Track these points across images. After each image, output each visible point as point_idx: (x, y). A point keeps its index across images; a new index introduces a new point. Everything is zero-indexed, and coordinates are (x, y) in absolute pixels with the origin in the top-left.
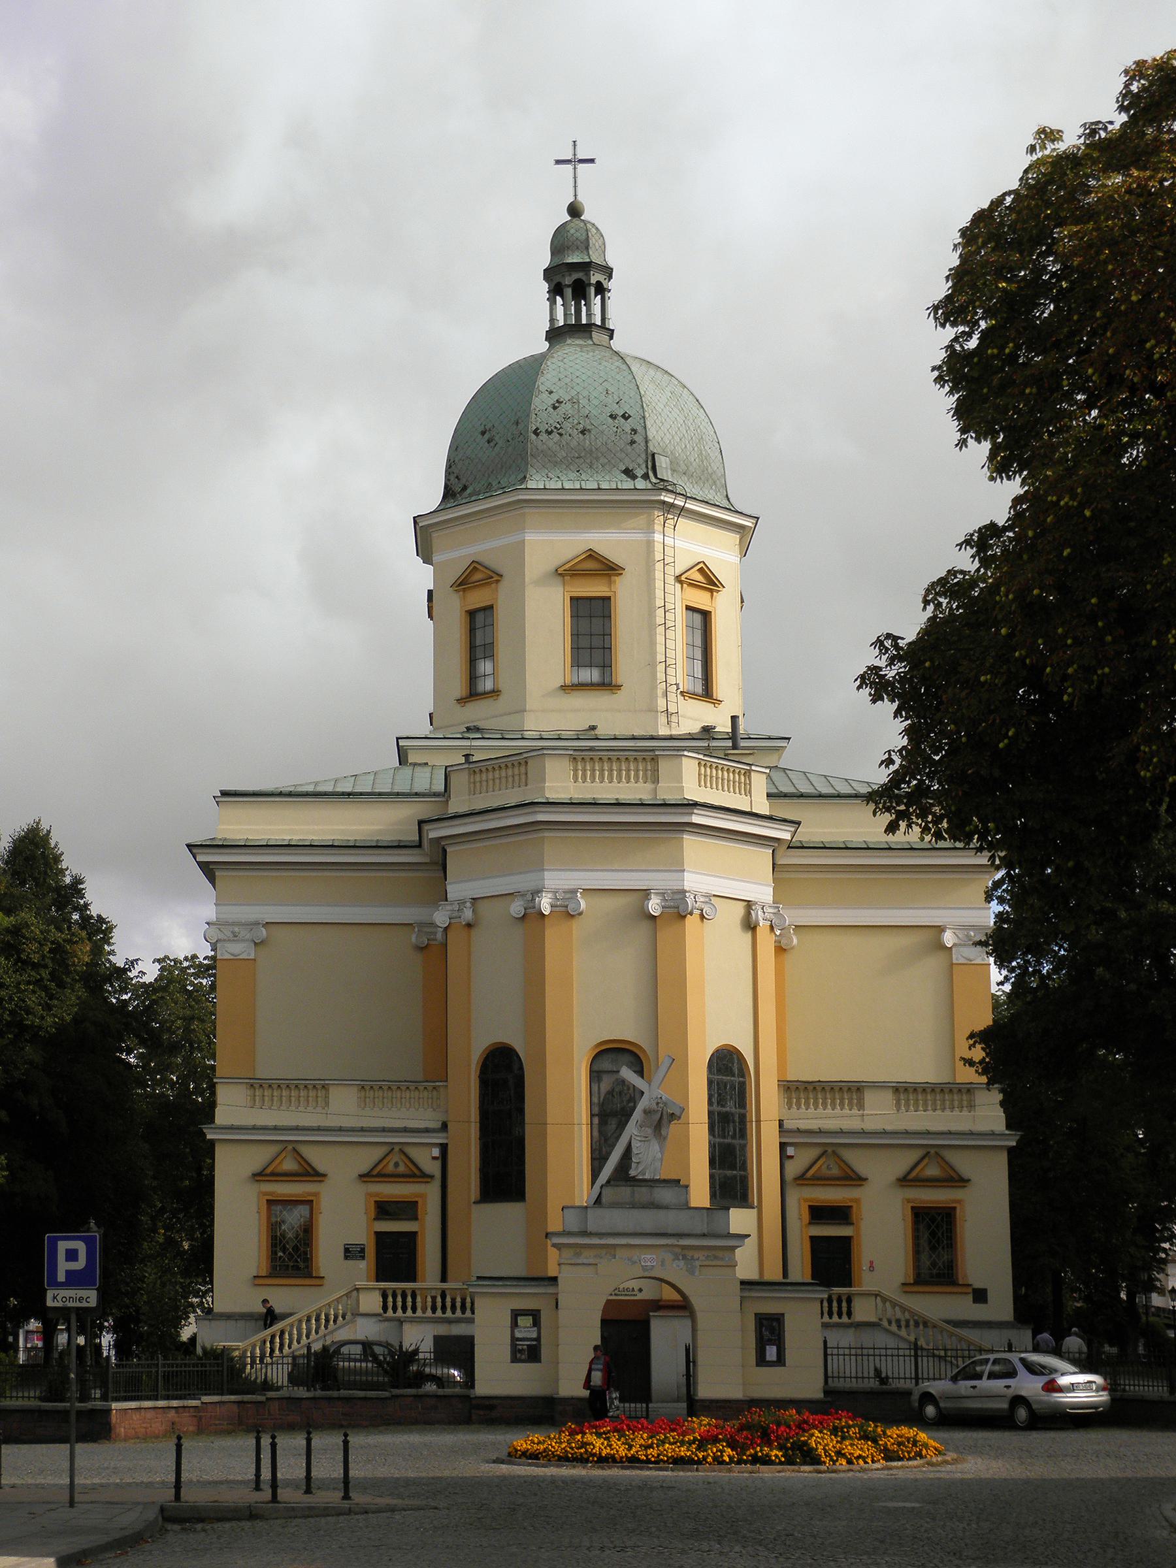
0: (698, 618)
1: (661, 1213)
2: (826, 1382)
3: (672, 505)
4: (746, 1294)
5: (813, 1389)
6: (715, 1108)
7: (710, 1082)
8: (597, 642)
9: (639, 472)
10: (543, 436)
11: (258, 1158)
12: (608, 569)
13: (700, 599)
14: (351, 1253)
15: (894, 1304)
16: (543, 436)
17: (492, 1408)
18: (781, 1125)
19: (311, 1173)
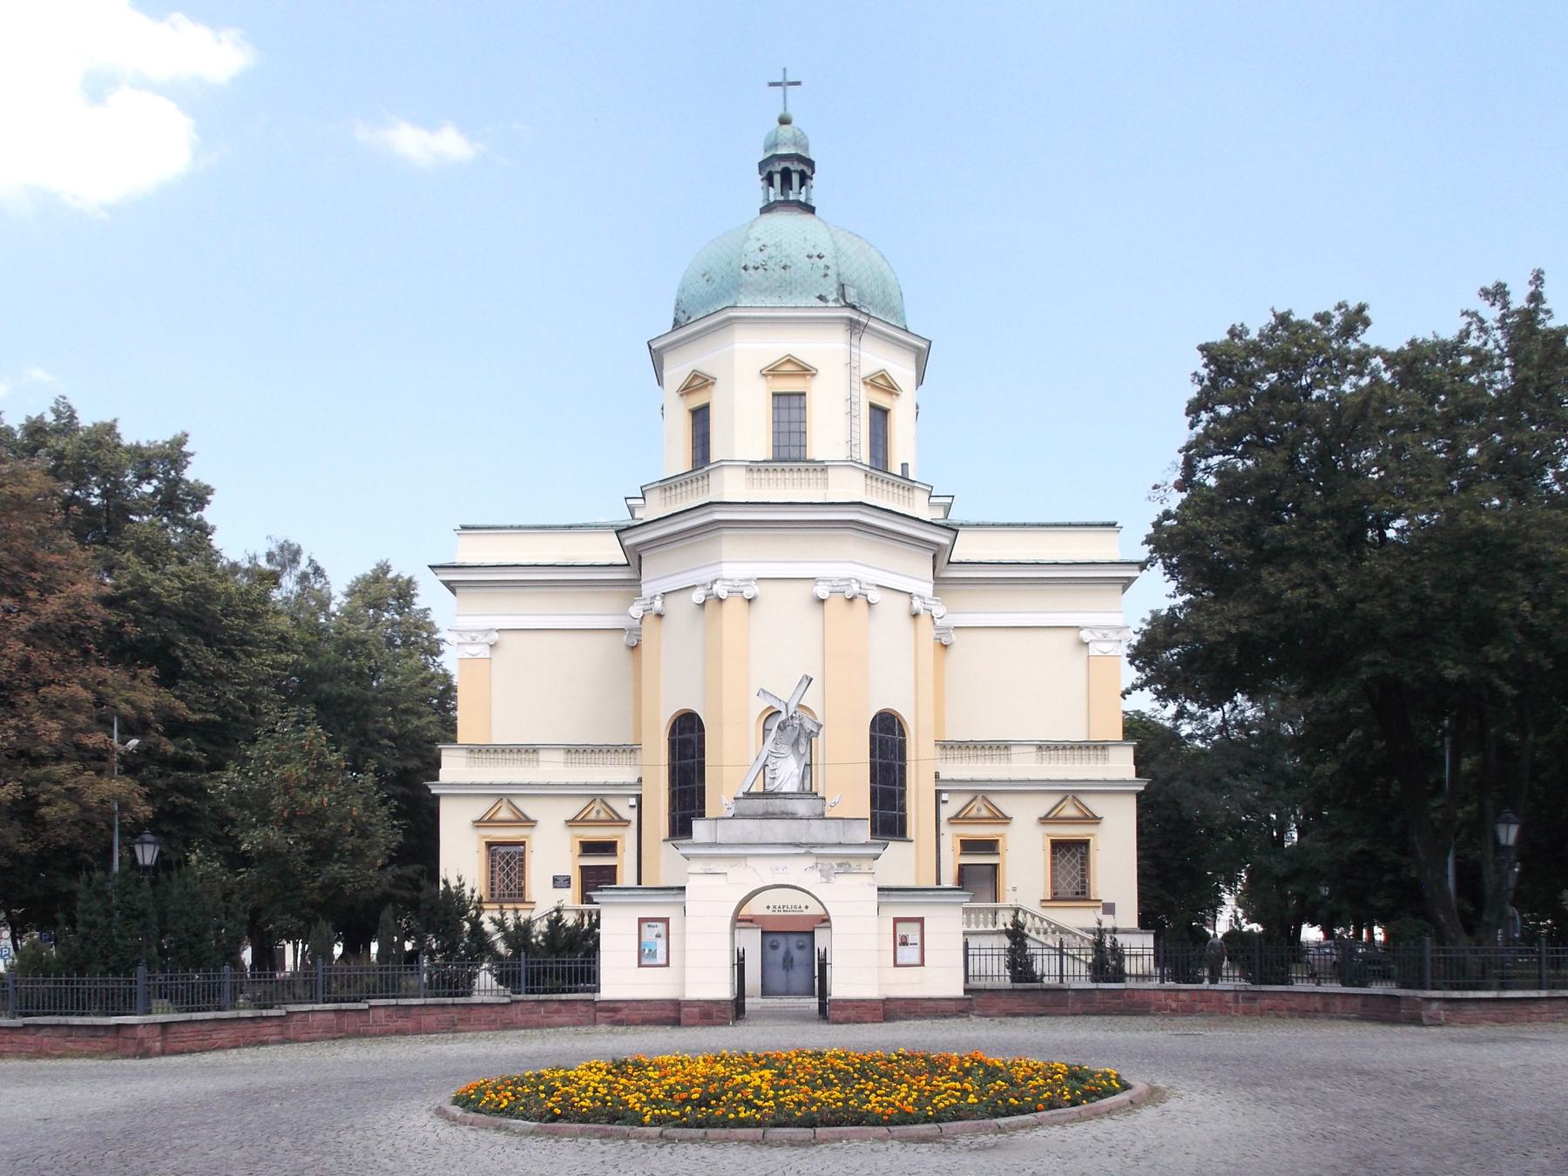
0: (879, 415)
1: (794, 824)
2: (966, 981)
3: (858, 323)
4: (884, 900)
5: (951, 986)
6: (878, 760)
7: (872, 739)
8: (794, 427)
9: (831, 298)
10: (751, 271)
11: (480, 808)
12: (805, 371)
13: (882, 400)
14: (560, 882)
15: (1033, 916)
16: (751, 271)
17: (615, 1010)
18: (937, 775)
19: (526, 822)
